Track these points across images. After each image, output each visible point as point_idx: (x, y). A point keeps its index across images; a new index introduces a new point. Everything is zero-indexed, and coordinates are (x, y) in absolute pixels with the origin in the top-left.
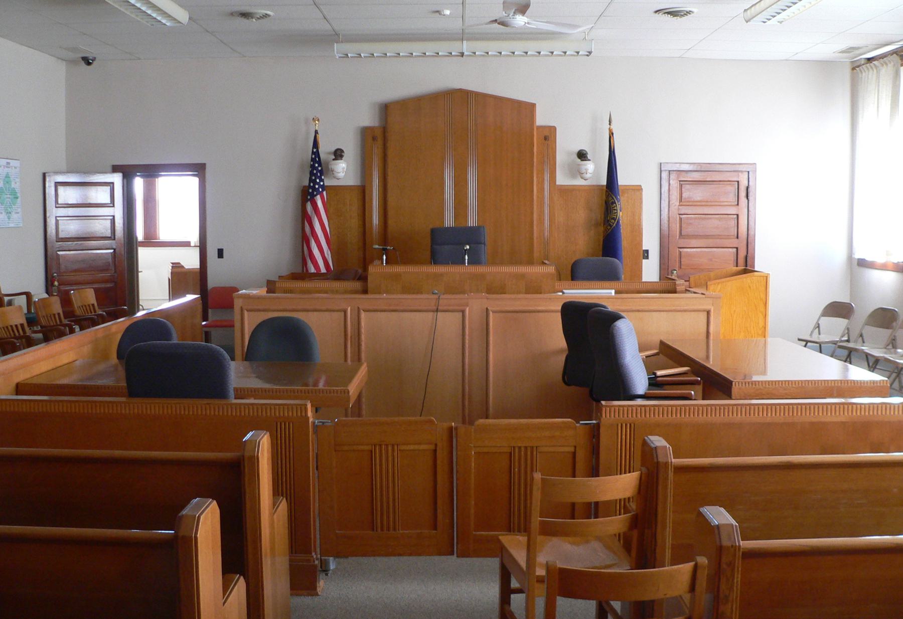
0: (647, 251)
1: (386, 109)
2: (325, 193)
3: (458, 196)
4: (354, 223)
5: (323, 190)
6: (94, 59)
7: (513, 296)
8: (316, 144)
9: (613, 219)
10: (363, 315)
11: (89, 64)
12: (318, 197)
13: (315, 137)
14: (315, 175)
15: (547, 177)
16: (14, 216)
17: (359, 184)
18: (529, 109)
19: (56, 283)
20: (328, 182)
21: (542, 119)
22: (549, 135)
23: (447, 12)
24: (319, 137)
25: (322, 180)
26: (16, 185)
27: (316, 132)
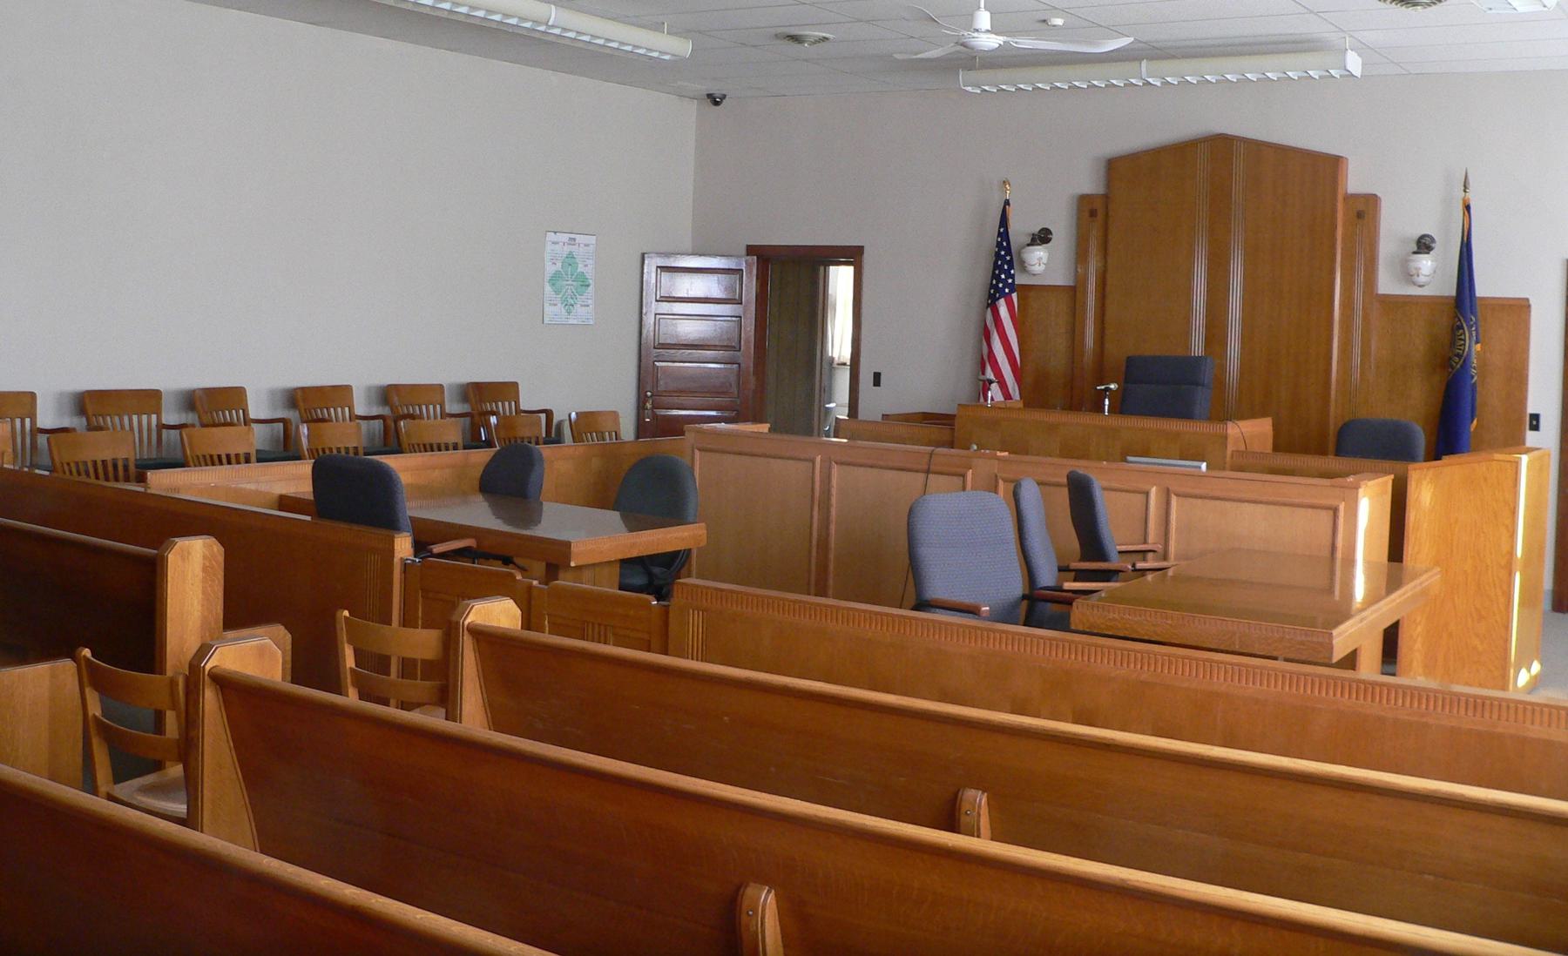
0: (1535, 417)
1: (1116, 168)
2: (1014, 296)
3: (1213, 306)
4: (1060, 344)
5: (1012, 291)
6: (724, 97)
7: (1034, 458)
8: (1004, 221)
9: (1460, 356)
10: (835, 469)
11: (716, 103)
12: (1002, 301)
13: (1004, 211)
14: (1000, 268)
15: (1360, 278)
16: (578, 309)
17: (1071, 284)
18: (1331, 166)
19: (649, 405)
20: (1020, 279)
21: (1356, 182)
22: (1365, 209)
23: (1059, 22)
24: (1011, 212)
25: (1012, 277)
26: (587, 268)
27: (1007, 203)
